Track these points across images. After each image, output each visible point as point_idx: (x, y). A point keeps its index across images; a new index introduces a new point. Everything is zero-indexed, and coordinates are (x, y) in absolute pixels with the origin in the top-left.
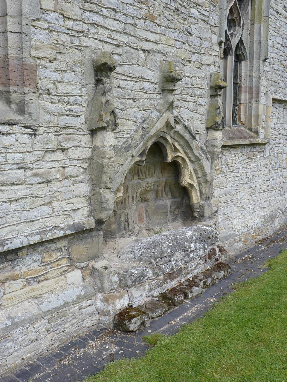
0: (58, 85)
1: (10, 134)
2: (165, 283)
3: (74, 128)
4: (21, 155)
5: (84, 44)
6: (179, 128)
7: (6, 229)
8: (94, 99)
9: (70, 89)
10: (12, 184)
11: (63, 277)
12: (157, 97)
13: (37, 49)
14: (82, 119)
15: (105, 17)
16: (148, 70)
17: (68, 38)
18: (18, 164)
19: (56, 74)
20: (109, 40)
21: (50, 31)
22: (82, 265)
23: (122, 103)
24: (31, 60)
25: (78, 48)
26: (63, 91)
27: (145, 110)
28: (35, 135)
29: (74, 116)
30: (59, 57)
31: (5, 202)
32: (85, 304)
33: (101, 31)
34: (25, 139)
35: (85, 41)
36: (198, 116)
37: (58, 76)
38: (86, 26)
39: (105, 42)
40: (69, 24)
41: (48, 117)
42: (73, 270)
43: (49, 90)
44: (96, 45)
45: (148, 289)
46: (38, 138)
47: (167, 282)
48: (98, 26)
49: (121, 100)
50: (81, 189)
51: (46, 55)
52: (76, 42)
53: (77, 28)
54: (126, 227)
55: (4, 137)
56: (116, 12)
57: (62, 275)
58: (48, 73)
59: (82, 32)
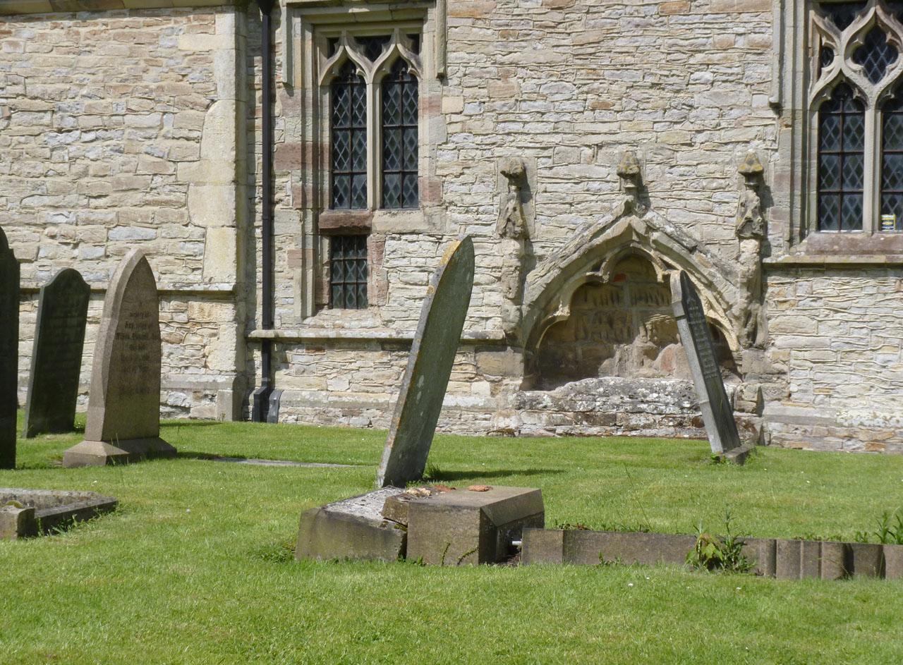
0: (465, 197)
1: (415, 241)
2: (576, 424)
3: (485, 236)
4: (424, 260)
5: (497, 154)
6: (655, 235)
7: (409, 322)
8: (829, 212)
9: (477, 199)
10: (416, 284)
11: (468, 384)
12: (618, 197)
13: (442, 168)
14: (494, 227)
15: (525, 123)
16: (597, 168)
17: (479, 153)
18: (420, 267)
19: (462, 187)
20: (531, 145)
21: (459, 150)
22: (492, 378)
23: (548, 209)
24: (436, 178)
25: (489, 159)
26: (470, 202)
27: (591, 215)
28: (440, 243)
29: (482, 224)
30: (465, 171)
31: (409, 299)
32: (481, 416)
33: (520, 137)
34: (428, 246)
35: (498, 151)
36: (714, 218)
37: (465, 189)
38: (500, 137)
39: (526, 148)
40: (478, 139)
41: (453, 226)
42: (480, 380)
43: (538, 201)
44: (511, 154)
45: (546, 420)
46: (442, 245)
47: (581, 424)
48: (516, 133)
49: (547, 206)
50: (492, 298)
51: (451, 172)
52: (488, 154)
53: (488, 141)
54: (612, 373)
55: (410, 244)
56: (543, 114)
57: (467, 381)
58: (454, 187)
59: (494, 144)
